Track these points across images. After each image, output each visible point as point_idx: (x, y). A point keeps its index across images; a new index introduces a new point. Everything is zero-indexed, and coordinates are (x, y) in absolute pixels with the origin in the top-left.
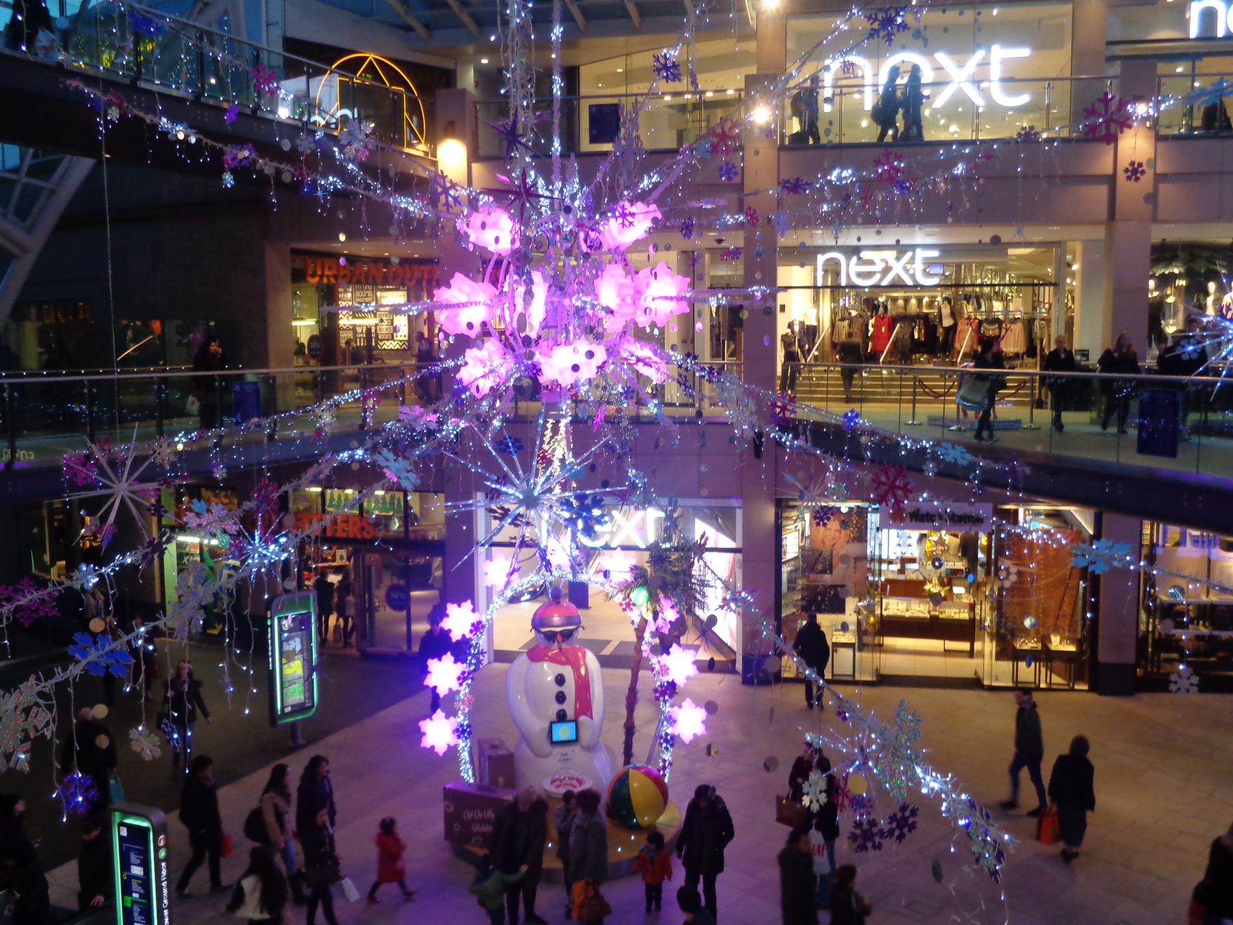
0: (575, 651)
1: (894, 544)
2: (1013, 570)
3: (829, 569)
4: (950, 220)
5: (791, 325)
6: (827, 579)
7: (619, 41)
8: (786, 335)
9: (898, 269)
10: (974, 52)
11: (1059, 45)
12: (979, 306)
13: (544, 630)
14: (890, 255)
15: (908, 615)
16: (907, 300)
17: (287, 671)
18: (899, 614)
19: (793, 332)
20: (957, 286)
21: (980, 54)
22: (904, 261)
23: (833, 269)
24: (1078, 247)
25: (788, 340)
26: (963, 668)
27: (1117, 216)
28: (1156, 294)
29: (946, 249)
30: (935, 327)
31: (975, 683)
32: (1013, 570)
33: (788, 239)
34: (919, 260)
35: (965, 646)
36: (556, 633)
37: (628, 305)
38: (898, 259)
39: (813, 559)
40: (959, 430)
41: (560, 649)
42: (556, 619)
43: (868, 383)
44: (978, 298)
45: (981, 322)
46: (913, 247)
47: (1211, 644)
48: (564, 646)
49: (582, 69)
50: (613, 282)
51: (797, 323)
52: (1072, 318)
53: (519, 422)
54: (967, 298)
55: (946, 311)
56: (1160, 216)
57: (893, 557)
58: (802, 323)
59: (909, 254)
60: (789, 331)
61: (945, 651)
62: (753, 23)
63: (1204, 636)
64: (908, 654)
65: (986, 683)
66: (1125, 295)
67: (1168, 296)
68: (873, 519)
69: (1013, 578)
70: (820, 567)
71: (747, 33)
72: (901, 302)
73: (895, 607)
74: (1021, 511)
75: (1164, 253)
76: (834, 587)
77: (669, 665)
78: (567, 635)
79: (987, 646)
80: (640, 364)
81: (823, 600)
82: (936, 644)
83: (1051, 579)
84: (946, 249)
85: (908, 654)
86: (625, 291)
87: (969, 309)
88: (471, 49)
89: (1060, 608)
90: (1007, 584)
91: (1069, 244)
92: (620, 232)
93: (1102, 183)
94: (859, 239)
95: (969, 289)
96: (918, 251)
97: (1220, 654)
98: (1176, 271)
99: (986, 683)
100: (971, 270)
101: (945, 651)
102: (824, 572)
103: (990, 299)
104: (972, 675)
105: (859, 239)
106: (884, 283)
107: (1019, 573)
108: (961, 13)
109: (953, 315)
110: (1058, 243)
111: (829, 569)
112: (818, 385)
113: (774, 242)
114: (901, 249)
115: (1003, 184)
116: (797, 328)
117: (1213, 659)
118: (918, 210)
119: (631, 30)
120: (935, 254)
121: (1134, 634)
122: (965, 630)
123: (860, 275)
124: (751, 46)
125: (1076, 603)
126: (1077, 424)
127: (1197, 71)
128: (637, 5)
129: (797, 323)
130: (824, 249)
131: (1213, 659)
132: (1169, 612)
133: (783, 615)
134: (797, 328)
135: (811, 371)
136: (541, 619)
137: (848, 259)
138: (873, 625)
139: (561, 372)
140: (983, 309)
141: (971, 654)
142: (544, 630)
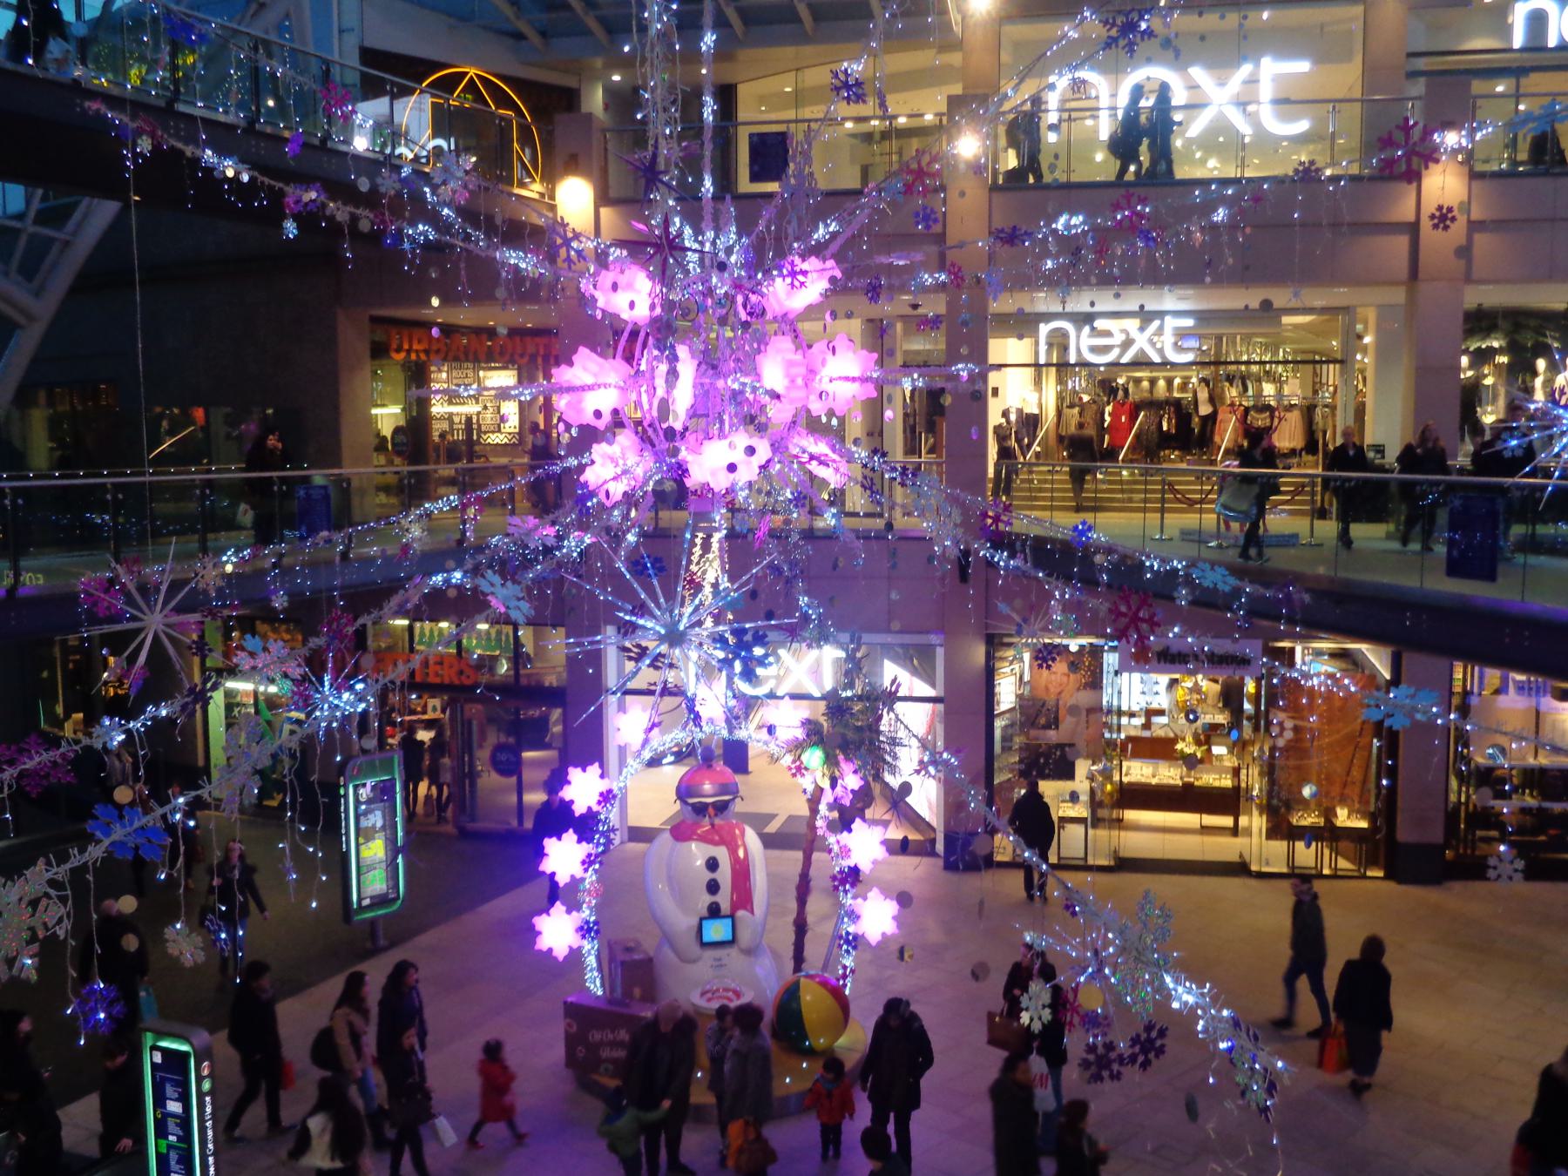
0: (732, 827)
1: (1137, 692)
2: (1289, 724)
3: (1054, 723)
4: (1208, 279)
5: (1005, 414)
6: (1052, 736)
7: (788, 52)
8: (1000, 426)
9: (1141, 342)
10: (1238, 66)
11: (1347, 57)
12: (1245, 389)
13: (691, 801)
14: (1132, 325)
15: (1154, 781)
16: (1153, 382)
17: (365, 853)
18: (1143, 780)
19: (1008, 422)
20: (1217, 363)
21: (1246, 69)
22: (1150, 332)
23: (1059, 342)
24: (1371, 315)
25: (1002, 433)
26: (1225, 849)
27: (1421, 275)
28: (1470, 373)
29: (1203, 317)
30: (1189, 416)
31: (1240, 869)
32: (1289, 724)
33: (1002, 304)
34: (1168, 331)
35: (1228, 821)
36: (707, 805)
37: (799, 388)
38: (1142, 329)
39: (1033, 711)
40: (1220, 546)
41: (713, 825)
42: (707, 787)
43: (1104, 487)
44: (1244, 379)
45: (1247, 410)
46: (1161, 314)
47: (1540, 819)
48: (717, 821)
49: (740, 88)
50: (779, 359)
51: (1013, 410)
52: (1363, 404)
53: (659, 536)
54: (1230, 379)
55: (1203, 395)
56: (1475, 275)
57: (1135, 708)
58: (1020, 411)
59: (1156, 323)
60: (1003, 420)
61: (1202, 827)
62: (957, 29)
63: (1531, 809)
64: (1154, 832)
65: (1254, 868)
66: (1430, 375)
67: (1485, 376)
68: (1111, 660)
69: (1289, 735)
70: (1043, 721)
71: (950, 43)
72: (1145, 384)
73: (1139, 771)
74: (1299, 649)
75: (1480, 321)
76: (1061, 746)
77: (851, 845)
78: (721, 808)
79: (1255, 821)
80: (814, 463)
81: (1046, 763)
82: (1190, 819)
83: (1337, 736)
84: (1203, 317)
85: (1154, 832)
86: (795, 371)
87: (1232, 393)
88: (599, 63)
89: (1348, 774)
90: (1281, 743)
91: (1359, 310)
92: (789, 295)
93: (1401, 233)
94: (1092, 304)
95: (1233, 368)
96: (1168, 319)
97: (1552, 832)
98: (1496, 344)
99: (1254, 868)
100: (1234, 343)
101: (1202, 827)
102: (1047, 727)
103: (1259, 380)
104: (1236, 858)
105: (1092, 304)
106: (1124, 360)
107: (1296, 729)
108: (1222, 17)
109: (1212, 400)
110: (1346, 309)
111: (1054, 723)
112: (1040, 490)
113: (985, 307)
114: (1146, 317)
115: (1276, 234)
116: (1013, 417)
117: (1543, 838)
118: (1168, 266)
119: (803, 39)
120: (1189, 322)
121: (1442, 806)
122: (1227, 801)
123: (1094, 349)
124: (955, 58)
125: (1368, 766)
126: (1369, 539)
127: (1522, 91)
128: (810, 6)
129: (1013, 410)
130: (1048, 317)
131: (1543, 838)
132: (1487, 777)
133: (996, 782)
134: (1013, 417)
135: (1031, 472)
136: (688, 787)
137: (1079, 330)
138: (1111, 794)
139: (713, 473)
140: (1250, 392)
141: (1235, 831)
142: (691, 801)
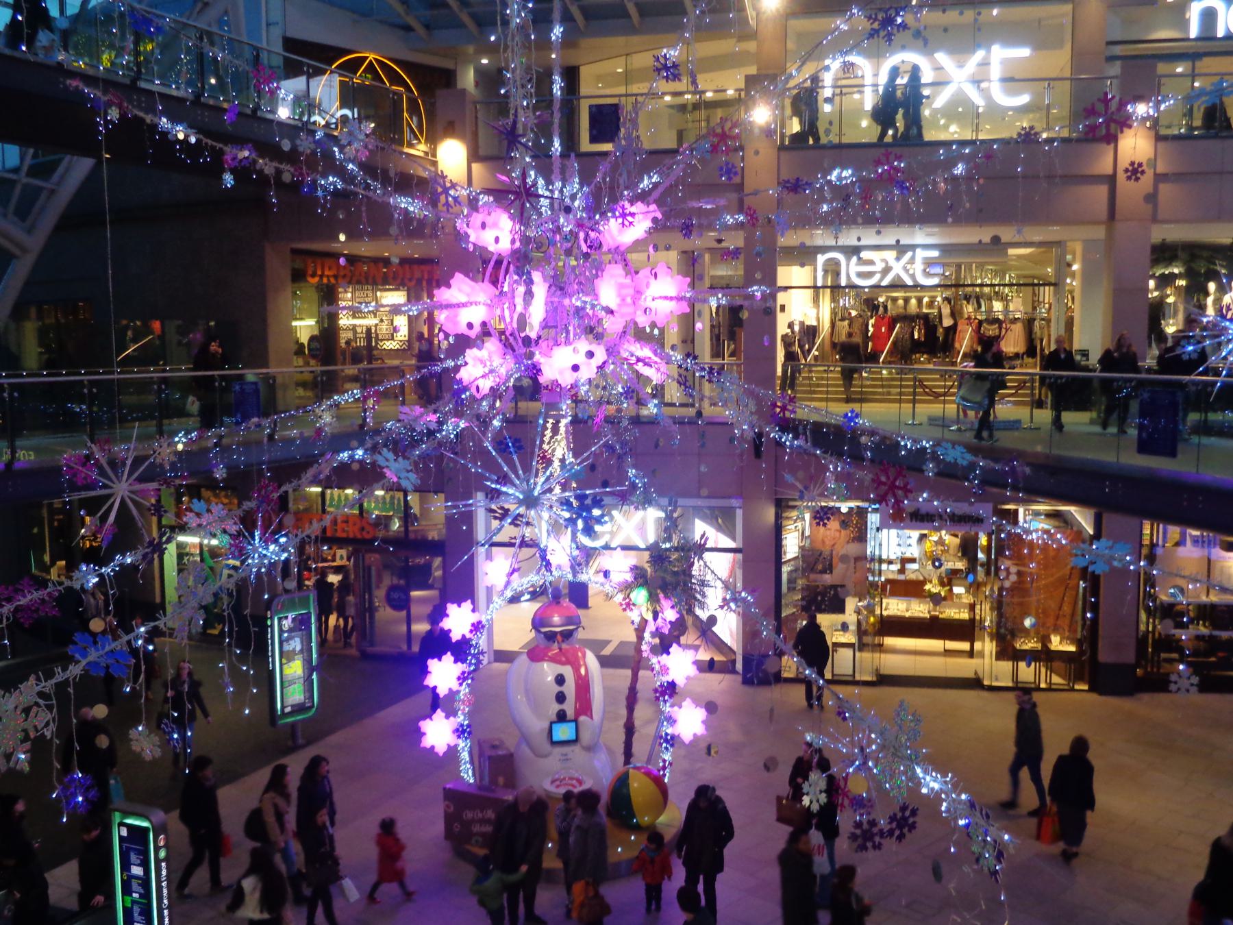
0: (575, 651)
1: (894, 544)
2: (1013, 570)
3: (829, 569)
4: (950, 220)
5: (791, 325)
6: (827, 579)
7: (619, 41)
8: (786, 335)
9: (898, 269)
10: (974, 52)
11: (1059, 45)
12: (979, 306)
13: (544, 630)
14: (890, 255)
15: (908, 615)
16: (907, 300)
17: (287, 671)
18: (899, 614)
19: (793, 332)
20: (957, 286)
21: (980, 54)
22: (904, 261)
23: (833, 269)
24: (1078, 247)
25: (788, 340)
26: (963, 668)
27: (1117, 216)
28: (1156, 294)
29: (946, 249)
30: (935, 327)
31: (975, 683)
32: (1013, 570)
33: (788, 239)
34: (919, 260)
35: (965, 646)
36: (556, 633)
37: (628, 305)
38: (898, 259)
39: (813, 559)
40: (959, 430)
41: (560, 649)
42: (556, 619)
43: (868, 383)
44: (978, 298)
45: (981, 322)
46: (913, 247)
47: (1211, 644)
48: (564, 646)
49: (582, 69)
50: (613, 282)
51: (797, 323)
52: (1072, 318)
53: (519, 422)
54: (967, 298)
55: (946, 311)
57: (893, 557)
58: (802, 323)
59: (909, 254)
60: (789, 331)
61: (945, 651)
62: (753, 23)
63: (1204, 636)
64: (908, 654)
65: (986, 683)
66: (1125, 295)
67: (1168, 296)
68: (873, 519)
69: (1013, 578)
70: (820, 567)
71: (747, 33)
72: (901, 302)
73: (895, 607)
74: (1021, 511)
75: (1164, 253)
76: (834, 587)
77: (669, 665)
78: (567, 635)
79: (987, 646)
80: (640, 364)
81: (823, 600)
82: (936, 644)
83: (1051, 579)
84: (946, 249)
85: (908, 654)
86: (625, 291)
87: (969, 309)
88: (471, 49)
89: (1060, 608)
90: (1007, 584)
91: (1069, 244)
92: (620, 232)
93: (1102, 183)
94: (859, 239)
95: (969, 289)
96: (918, 251)
97: (1220, 654)
98: (1176, 271)
99: (986, 683)
100: (971, 270)
101: (945, 651)
102: (824, 572)
103: (990, 299)
104: (972, 675)
105: (859, 239)
106: (884, 283)
107: (1019, 573)
108: (961, 13)
109: (953, 315)
110: (1058, 243)
111: (829, 569)
112: (818, 385)
113: (774, 242)
114: (901, 249)
115: (1003, 184)
116: (797, 328)
117: (1213, 659)
118: (918, 210)
119: (631, 30)
120: (935, 254)
121: (1134, 634)
122: (965, 630)
123: (860, 275)
124: (751, 46)
125: (1076, 603)
126: (1077, 424)
127: (1197, 71)
128: (637, 5)
129: (797, 323)
130: (824, 249)
131: (1213, 659)
132: (1169, 612)
133: (783, 615)
134: (797, 328)
135: (811, 371)
136: (541, 619)
137: (848, 259)
138: (873, 625)
139: (561, 372)
140: (983, 309)
141: (971, 654)
142: (544, 630)
